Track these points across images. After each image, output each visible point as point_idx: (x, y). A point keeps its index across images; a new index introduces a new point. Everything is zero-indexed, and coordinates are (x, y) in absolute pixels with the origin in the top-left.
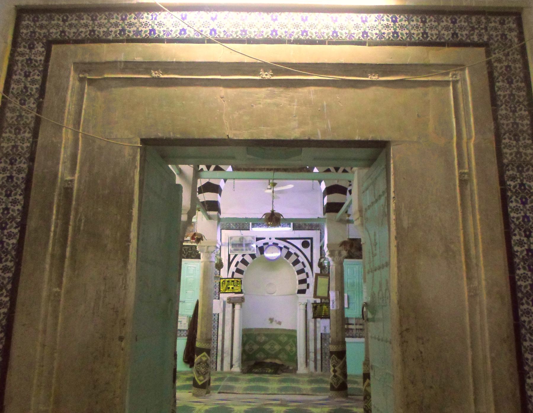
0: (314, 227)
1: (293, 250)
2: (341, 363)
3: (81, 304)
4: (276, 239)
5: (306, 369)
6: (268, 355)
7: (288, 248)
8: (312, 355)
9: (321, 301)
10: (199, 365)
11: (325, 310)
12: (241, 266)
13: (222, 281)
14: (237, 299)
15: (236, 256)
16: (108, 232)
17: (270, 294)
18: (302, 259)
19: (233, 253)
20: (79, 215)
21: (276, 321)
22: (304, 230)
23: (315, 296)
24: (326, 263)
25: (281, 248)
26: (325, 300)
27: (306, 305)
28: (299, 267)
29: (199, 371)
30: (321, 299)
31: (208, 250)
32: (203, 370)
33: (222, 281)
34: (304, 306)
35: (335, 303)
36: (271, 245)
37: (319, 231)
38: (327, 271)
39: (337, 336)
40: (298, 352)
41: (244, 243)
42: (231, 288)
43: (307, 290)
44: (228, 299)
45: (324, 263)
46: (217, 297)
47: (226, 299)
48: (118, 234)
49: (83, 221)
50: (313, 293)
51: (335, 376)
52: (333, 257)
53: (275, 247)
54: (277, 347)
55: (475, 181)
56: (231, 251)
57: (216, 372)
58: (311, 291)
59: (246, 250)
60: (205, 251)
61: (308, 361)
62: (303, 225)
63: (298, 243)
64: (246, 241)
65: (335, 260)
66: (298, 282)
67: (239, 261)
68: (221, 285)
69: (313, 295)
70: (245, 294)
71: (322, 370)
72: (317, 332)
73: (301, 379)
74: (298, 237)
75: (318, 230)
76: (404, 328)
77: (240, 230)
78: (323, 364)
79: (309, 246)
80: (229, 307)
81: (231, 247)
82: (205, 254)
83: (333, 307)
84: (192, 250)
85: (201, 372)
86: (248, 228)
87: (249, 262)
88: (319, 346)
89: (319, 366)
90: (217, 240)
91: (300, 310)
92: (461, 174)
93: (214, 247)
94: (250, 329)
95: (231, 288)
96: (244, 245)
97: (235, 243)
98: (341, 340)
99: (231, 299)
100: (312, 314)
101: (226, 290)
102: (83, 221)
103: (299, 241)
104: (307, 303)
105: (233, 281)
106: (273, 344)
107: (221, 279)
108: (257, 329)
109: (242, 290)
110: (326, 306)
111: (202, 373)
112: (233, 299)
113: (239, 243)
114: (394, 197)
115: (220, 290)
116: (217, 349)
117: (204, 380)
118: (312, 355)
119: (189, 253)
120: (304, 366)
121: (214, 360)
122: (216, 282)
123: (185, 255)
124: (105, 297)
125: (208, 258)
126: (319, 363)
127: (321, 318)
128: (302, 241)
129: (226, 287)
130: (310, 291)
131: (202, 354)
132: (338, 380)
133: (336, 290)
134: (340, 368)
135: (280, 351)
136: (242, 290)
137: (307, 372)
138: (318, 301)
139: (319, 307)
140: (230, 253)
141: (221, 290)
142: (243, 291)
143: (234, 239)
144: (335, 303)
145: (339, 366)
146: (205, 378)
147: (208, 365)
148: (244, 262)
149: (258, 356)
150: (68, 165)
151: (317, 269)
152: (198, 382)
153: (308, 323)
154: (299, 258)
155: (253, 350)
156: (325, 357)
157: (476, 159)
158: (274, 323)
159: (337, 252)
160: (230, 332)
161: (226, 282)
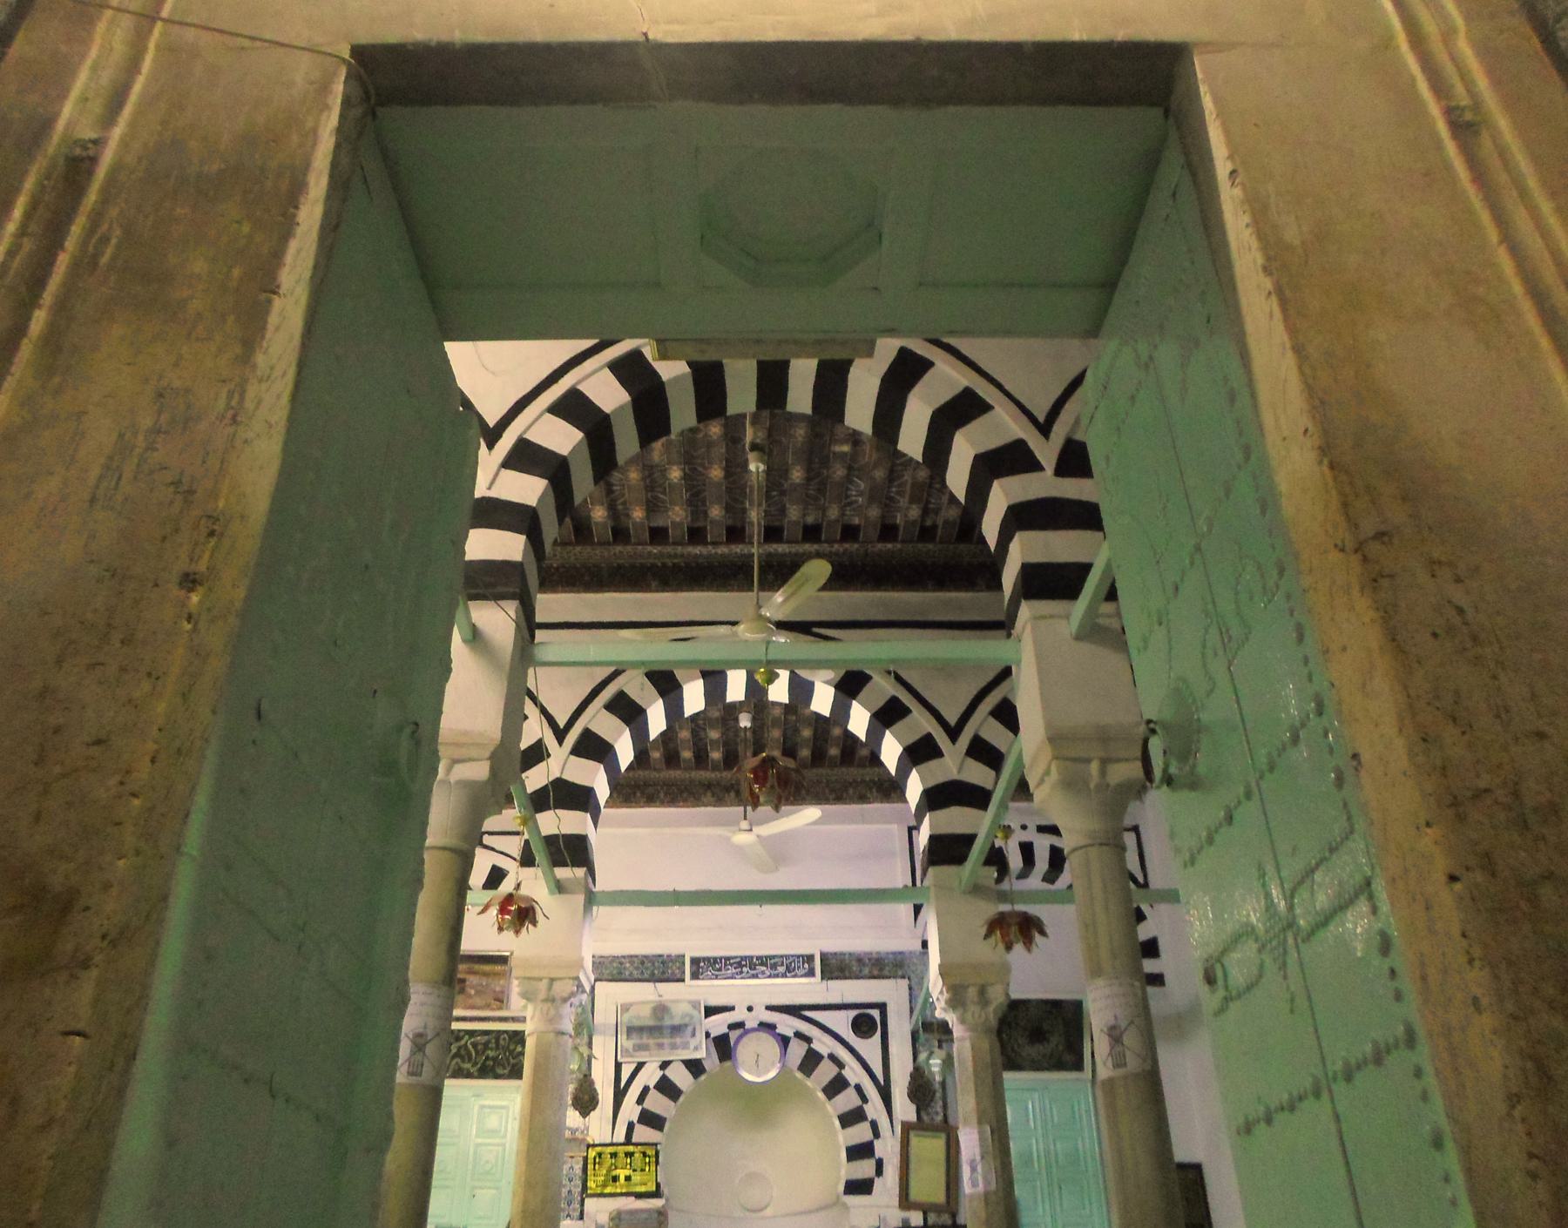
0: (887, 968)
1: (824, 1044)
3: (52, 474)
4: (770, 1008)
7: (808, 1040)
9: (925, 1220)
12: (657, 1102)
13: (592, 1153)
14: (644, 1216)
15: (640, 1066)
16: (199, 266)
18: (854, 1073)
19: (632, 1056)
20: (105, 227)
22: (858, 978)
23: (905, 1202)
24: (935, 1065)
25: (784, 1041)
26: (939, 1216)
28: (848, 1100)
30: (925, 1214)
31: (552, 993)
37: (904, 983)
38: (937, 1113)
42: (622, 1178)
43: (878, 1182)
44: (612, 1219)
45: (929, 1065)
48: (236, 272)
49: (114, 241)
50: (897, 1191)
52: (960, 1010)
55: (1503, 123)
56: (626, 1052)
59: (674, 1047)
60: (542, 996)
62: (854, 963)
63: (841, 1022)
65: (969, 1016)
66: (844, 1155)
68: (590, 1167)
76: (1369, 526)
81: (625, 1037)
83: (974, 1184)
84: (497, 1048)
86: (678, 976)
90: (582, 959)
92: (1451, 113)
93: (571, 981)
95: (622, 1178)
97: (637, 1023)
101: (604, 1186)
102: (114, 241)
105: (629, 1155)
107: (589, 1146)
109: (658, 1185)
113: (651, 1023)
114: (1233, 173)
115: (585, 1187)
119: (487, 1058)
122: (572, 1157)
123: (475, 1064)
124: (151, 448)
128: (853, 1013)
129: (606, 1175)
130: (888, 1184)
133: (980, 1122)
136: (658, 1185)
140: (622, 1056)
141: (591, 1184)
142: (665, 1189)
148: (667, 1087)
150: (97, 107)
151: (904, 1109)
154: (846, 1073)
157: (1490, 73)
159: (972, 992)
161: (608, 1161)
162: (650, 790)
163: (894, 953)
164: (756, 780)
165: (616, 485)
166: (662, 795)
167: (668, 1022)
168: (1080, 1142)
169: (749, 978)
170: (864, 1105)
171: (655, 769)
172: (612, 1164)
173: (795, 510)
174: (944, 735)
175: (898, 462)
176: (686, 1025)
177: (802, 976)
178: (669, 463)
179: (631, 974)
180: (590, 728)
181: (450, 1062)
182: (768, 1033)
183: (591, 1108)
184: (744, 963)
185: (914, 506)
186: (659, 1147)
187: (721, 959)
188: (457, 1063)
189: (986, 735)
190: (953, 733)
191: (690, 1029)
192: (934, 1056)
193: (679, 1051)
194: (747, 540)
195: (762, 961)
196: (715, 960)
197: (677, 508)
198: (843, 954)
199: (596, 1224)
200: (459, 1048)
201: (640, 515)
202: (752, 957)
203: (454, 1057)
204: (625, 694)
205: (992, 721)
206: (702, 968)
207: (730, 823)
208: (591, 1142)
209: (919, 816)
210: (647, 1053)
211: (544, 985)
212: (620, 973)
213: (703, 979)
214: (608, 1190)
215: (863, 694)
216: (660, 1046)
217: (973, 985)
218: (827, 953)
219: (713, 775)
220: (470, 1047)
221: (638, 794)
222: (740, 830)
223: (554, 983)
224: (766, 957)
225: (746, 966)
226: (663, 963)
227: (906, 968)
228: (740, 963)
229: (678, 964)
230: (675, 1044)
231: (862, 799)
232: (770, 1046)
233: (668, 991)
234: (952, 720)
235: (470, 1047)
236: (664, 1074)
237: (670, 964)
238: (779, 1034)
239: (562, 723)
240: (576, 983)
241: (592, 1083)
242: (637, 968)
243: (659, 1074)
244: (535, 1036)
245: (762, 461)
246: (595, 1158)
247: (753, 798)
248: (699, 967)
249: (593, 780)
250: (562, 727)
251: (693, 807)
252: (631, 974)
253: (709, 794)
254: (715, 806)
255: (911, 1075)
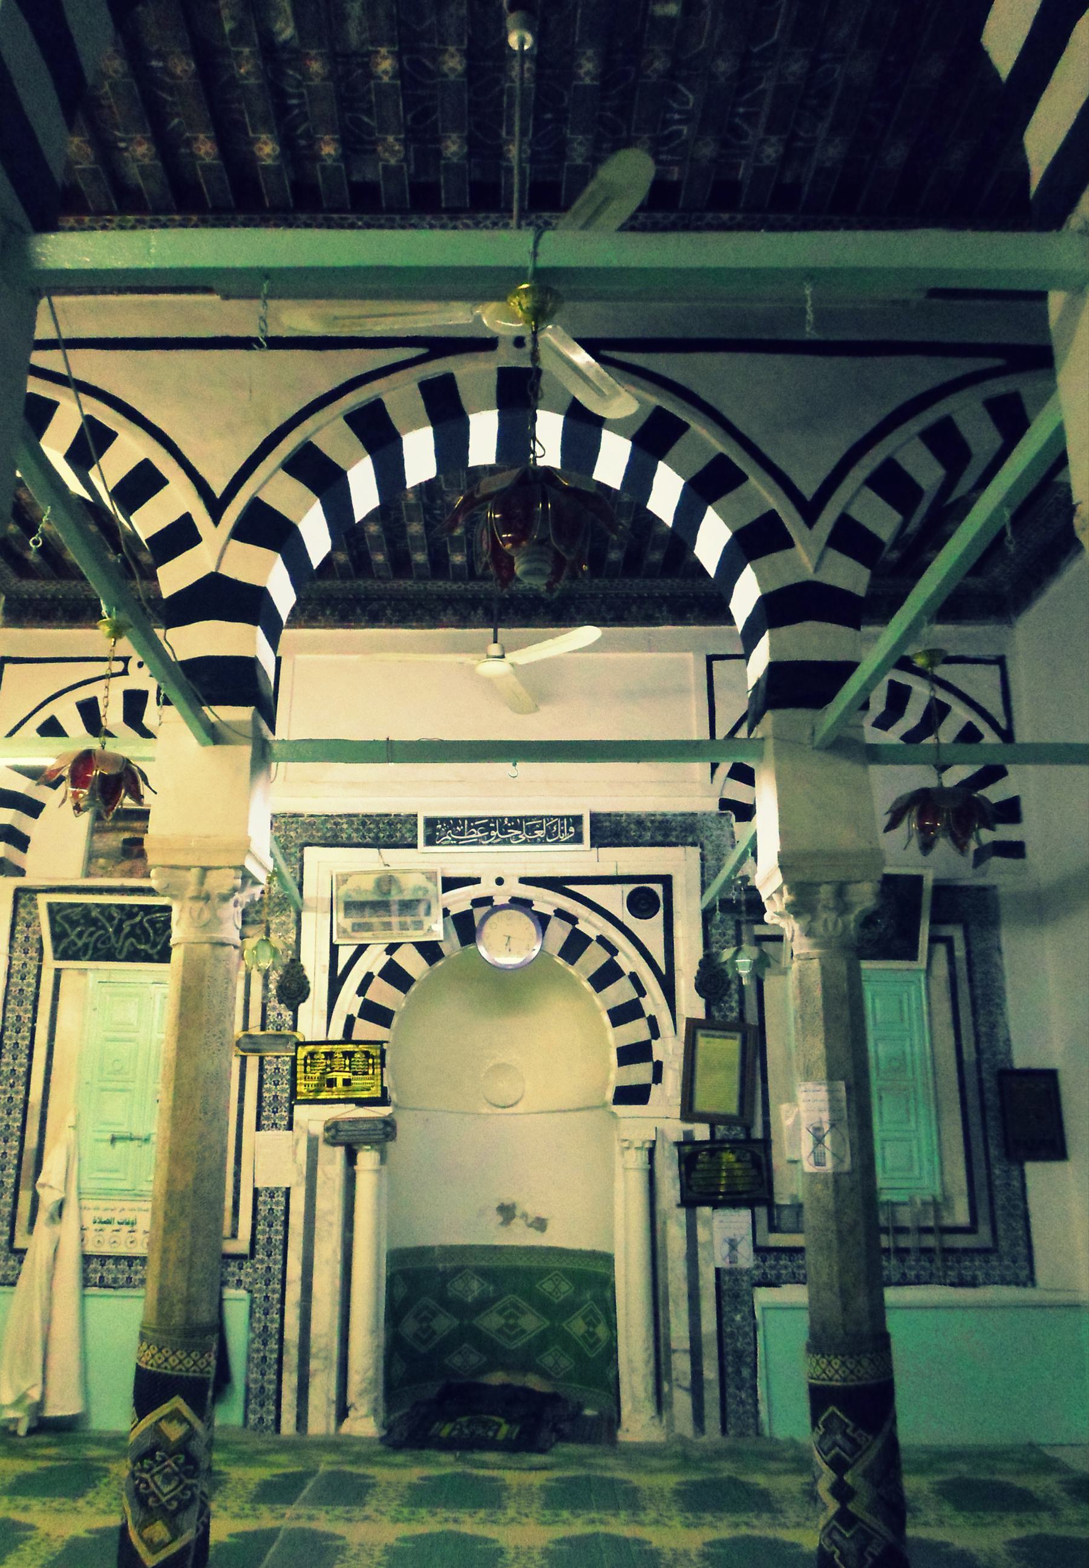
1: (591, 925)
2: (878, 1444)
4: (524, 881)
5: (656, 1421)
6: (496, 1356)
7: (572, 919)
8: (682, 1364)
10: (147, 1463)
11: (729, 1170)
12: (383, 993)
13: (302, 1052)
14: (365, 1126)
15: (361, 949)
17: (498, 1106)
18: (629, 960)
19: (351, 937)
21: (525, 1216)
23: (688, 1113)
27: (651, 1152)
28: (620, 992)
29: (147, 1496)
32: (166, 1489)
33: (302, 1052)
34: (644, 1156)
35: (827, 1140)
36: (503, 907)
38: (731, 1009)
39: (845, 1309)
40: (620, 1348)
41: (395, 897)
42: (340, 1082)
43: (655, 1090)
44: (327, 1129)
46: (282, 1118)
47: (318, 1129)
51: (844, 1517)
52: (808, 918)
53: (516, 915)
54: (531, 1323)
57: (276, 1437)
58: (669, 1093)
59: (403, 927)
60: (192, 890)
61: (666, 1387)
62: (632, 826)
63: (614, 898)
64: (401, 891)
65: (819, 926)
66: (614, 1058)
67: (376, 973)
68: (300, 1068)
69: (677, 1112)
70: (396, 1106)
71: (724, 1431)
72: (701, 1263)
73: (640, 1480)
74: (610, 871)
75: (694, 844)
77: (379, 847)
78: (729, 1400)
79: (657, 910)
80: (332, 1160)
81: (341, 914)
82: (189, 904)
85: (158, 1500)
87: (415, 976)
88: (709, 1324)
89: (712, 1412)
91: (626, 1169)
93: (232, 872)
94: (422, 1252)
95: (340, 1082)
96: (395, 908)
98: (866, 1328)
99: (341, 1127)
100: (678, 1186)
101: (318, 1091)
103: (618, 888)
104: (654, 1142)
105: (348, 1055)
106: (517, 1307)
108: (450, 1252)
109: (384, 1090)
110: (733, 1152)
111: (163, 1508)
112: (346, 1127)
115: (294, 1093)
116: (281, 1340)
117: (174, 1539)
118: (682, 1364)
120: (650, 1409)
121: (266, 1386)
122: (277, 1057)
125: (205, 926)
126: (712, 1395)
127: (716, 1205)
128: (629, 888)
131: (165, 1409)
132: (865, 1536)
133: (831, 1077)
134: (866, 1474)
135: (543, 1340)
136: (384, 1090)
137: (663, 1439)
138: (701, 1132)
139: (703, 1157)
141: (301, 1088)
142: (393, 1095)
143: (351, 884)
144: (827, 1140)
145: (859, 1468)
146: (176, 1532)
147: (191, 1460)
148: (395, 975)
149: (456, 1360)
152: (141, 1549)
153: (659, 1226)
154: (620, 959)
155: (434, 1333)
156: (738, 1372)
158: (516, 1220)
159: (825, 892)
160: (338, 1269)
162: (375, 606)
163: (683, 815)
164: (507, 523)
165: (293, 96)
166: (389, 612)
167: (395, 897)
168: (908, 1044)
169: (499, 843)
170: (641, 999)
171: (380, 578)
172: (327, 1066)
173: (580, 143)
174: (797, 517)
175: (756, 50)
176: (418, 901)
177: (566, 842)
178: (376, 41)
179: (349, 837)
180: (261, 498)
181: (123, 943)
182: (520, 910)
183: (300, 999)
184: (492, 825)
185: (773, 139)
186: (385, 1046)
187: (463, 819)
188: (132, 944)
189: (857, 513)
190: (810, 512)
191: (422, 908)
192: (741, 954)
193: (409, 933)
194: (503, 205)
195: (516, 822)
196: (456, 820)
197: (391, 139)
198: (618, 815)
199: (309, 1133)
200: (133, 926)
201: (333, 152)
202: (503, 818)
203: (127, 937)
204: (316, 448)
205: (869, 494)
206: (439, 830)
207: (479, 649)
208: (302, 1040)
209: (750, 637)
210: (369, 934)
211: (193, 876)
212: (336, 836)
213: (440, 844)
214: (323, 1096)
215: (676, 450)
216: (388, 926)
217: (827, 883)
218: (599, 814)
219: (455, 587)
220: (147, 925)
221: (359, 611)
222: (488, 657)
223: (209, 873)
224: (521, 818)
225: (494, 829)
226: (390, 824)
227: (698, 832)
228: (486, 825)
229: (409, 826)
230: (405, 923)
231: (649, 620)
232: (521, 925)
233: (396, 858)
234: (808, 489)
235: (147, 925)
236: (391, 959)
237: (399, 826)
238: (537, 913)
239: (218, 490)
240: (240, 874)
241: (302, 969)
242: (357, 830)
243: (385, 958)
244: (182, 947)
245: (530, 29)
246: (305, 1059)
247: (498, 567)
248: (435, 830)
249: (266, 577)
250: (218, 496)
251: (430, 627)
252: (349, 837)
253: (450, 612)
254: (457, 627)
255: (701, 963)
